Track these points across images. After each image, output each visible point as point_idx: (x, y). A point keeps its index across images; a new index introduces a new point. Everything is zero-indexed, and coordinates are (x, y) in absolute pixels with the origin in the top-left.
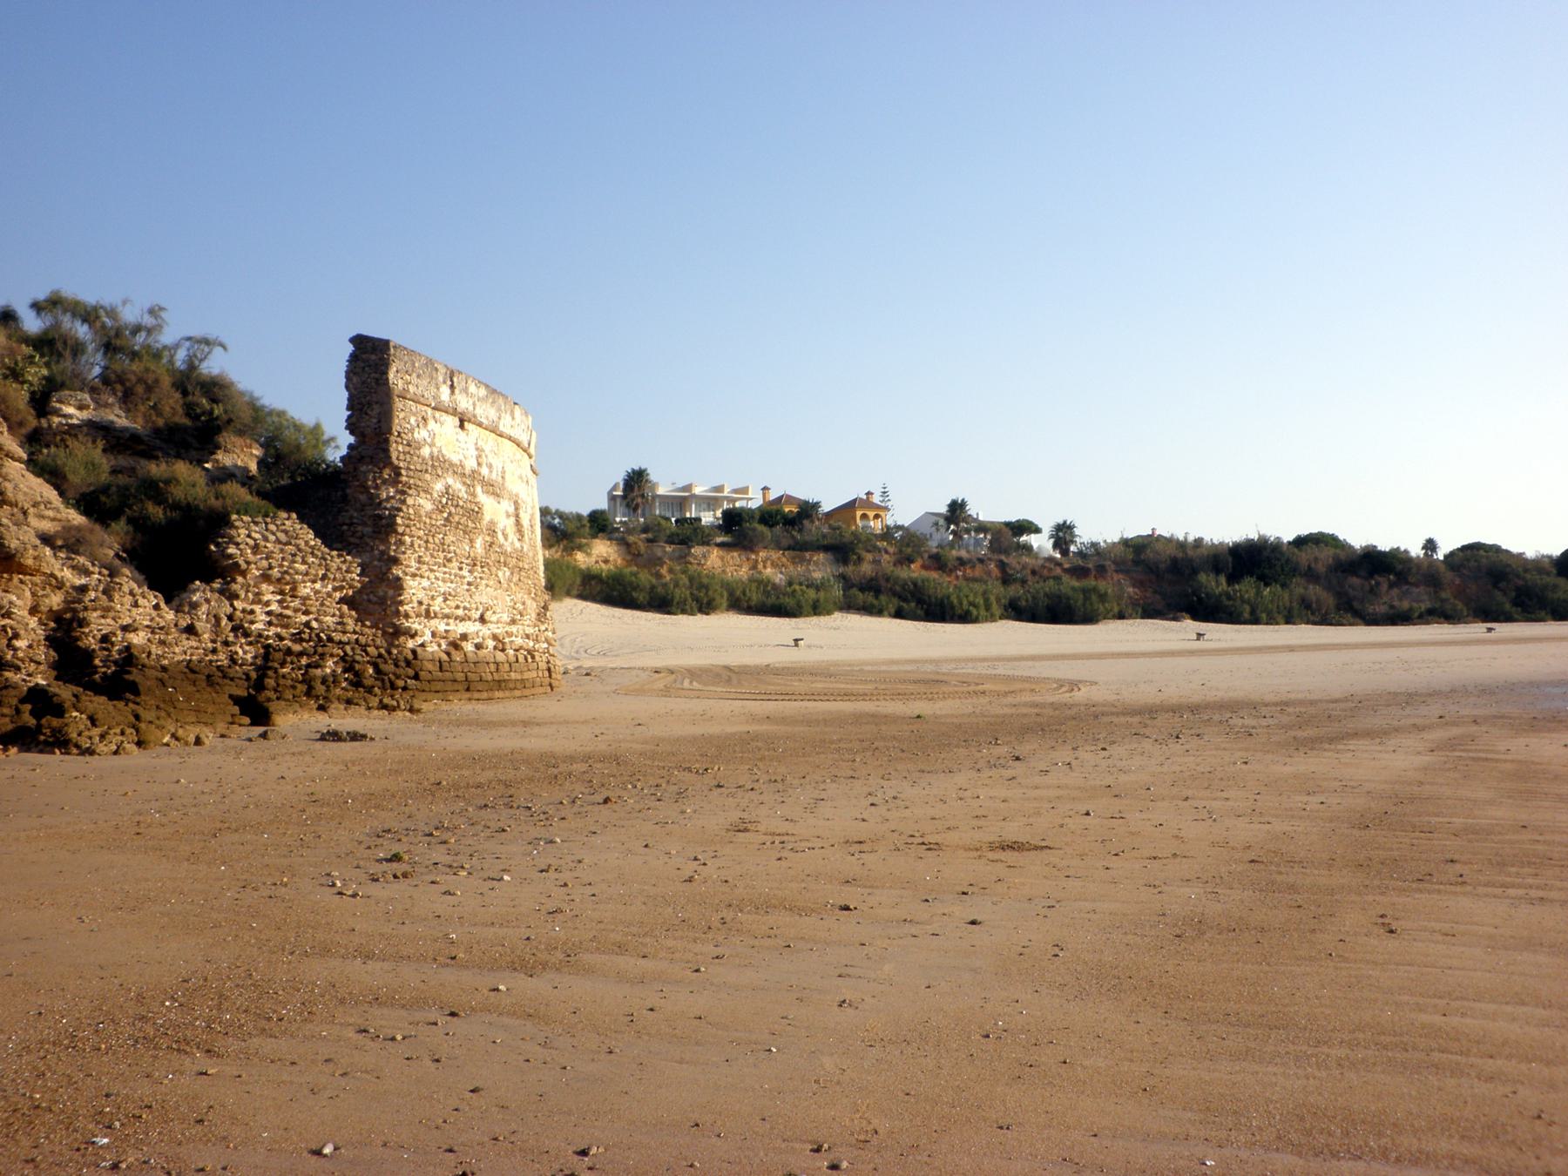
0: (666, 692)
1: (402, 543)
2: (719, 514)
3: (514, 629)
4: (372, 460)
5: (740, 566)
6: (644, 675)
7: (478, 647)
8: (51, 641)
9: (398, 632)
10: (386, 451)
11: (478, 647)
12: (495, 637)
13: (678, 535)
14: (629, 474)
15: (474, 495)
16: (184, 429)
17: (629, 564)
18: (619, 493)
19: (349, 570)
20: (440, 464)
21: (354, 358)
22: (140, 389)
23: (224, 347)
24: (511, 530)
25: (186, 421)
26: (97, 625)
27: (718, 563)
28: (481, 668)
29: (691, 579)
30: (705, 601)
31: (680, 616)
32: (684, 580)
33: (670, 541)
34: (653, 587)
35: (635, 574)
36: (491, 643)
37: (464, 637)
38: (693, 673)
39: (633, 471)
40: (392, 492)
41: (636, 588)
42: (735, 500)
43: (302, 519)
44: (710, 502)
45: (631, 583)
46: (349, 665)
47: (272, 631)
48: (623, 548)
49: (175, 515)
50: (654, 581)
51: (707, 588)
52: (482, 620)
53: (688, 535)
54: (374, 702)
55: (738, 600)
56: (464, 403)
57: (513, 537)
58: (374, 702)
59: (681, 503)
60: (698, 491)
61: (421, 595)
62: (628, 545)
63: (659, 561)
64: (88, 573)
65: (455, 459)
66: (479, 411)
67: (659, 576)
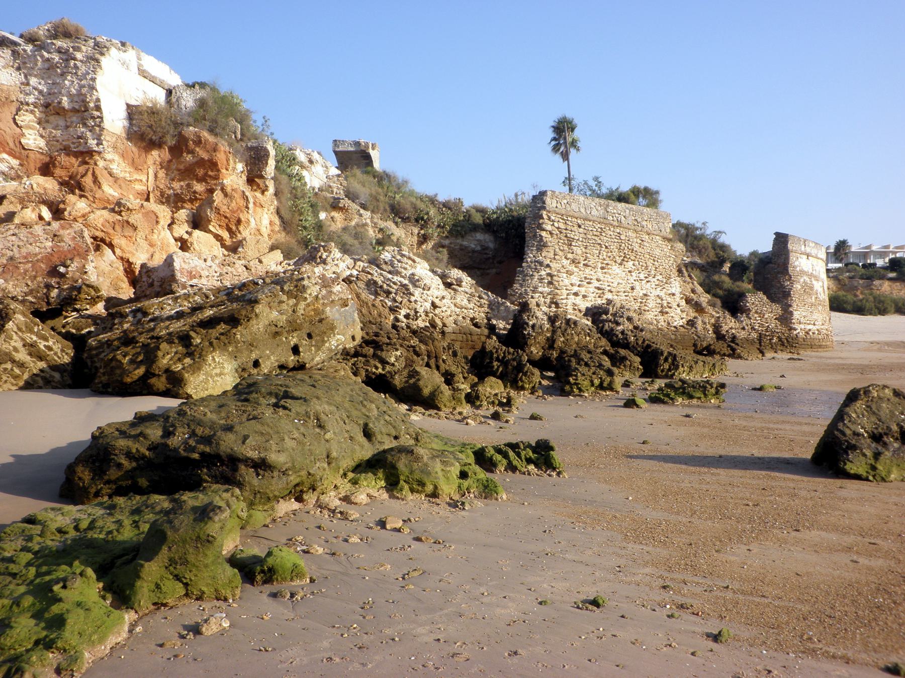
0: (880, 350)
1: (792, 300)
2: (887, 260)
3: (822, 327)
4: (782, 273)
5: (901, 290)
6: (867, 344)
7: (813, 333)
8: (714, 332)
9: (791, 329)
10: (787, 270)
11: (813, 333)
12: (818, 330)
13: (866, 275)
14: (837, 243)
15: (811, 281)
16: (716, 262)
17: (839, 289)
18: (832, 250)
19: (777, 309)
20: (803, 272)
21: (775, 239)
22: (703, 250)
23: (578, 150)
24: (822, 293)
25: (716, 259)
26: (725, 328)
27: (888, 289)
28: (815, 341)
29: (875, 298)
30: (883, 308)
31: (869, 317)
32: (871, 298)
33: (862, 278)
34: (854, 302)
35: (845, 296)
36: (817, 332)
37: (810, 330)
38: (888, 344)
39: (840, 241)
40: (788, 283)
41: (846, 302)
42: (896, 252)
43: (764, 294)
44: (882, 255)
45: (843, 300)
46: (780, 339)
47: (760, 329)
48: (837, 282)
49: (726, 293)
50: (855, 299)
51: (883, 302)
52: (814, 324)
53: (870, 273)
54: (788, 351)
55: (900, 308)
56: (808, 250)
57: (822, 295)
58: (788, 351)
59: (865, 255)
60: (874, 248)
61: (798, 317)
62: (839, 280)
63: (856, 288)
64: (719, 313)
65: (806, 270)
66: (812, 252)
67: (856, 296)
